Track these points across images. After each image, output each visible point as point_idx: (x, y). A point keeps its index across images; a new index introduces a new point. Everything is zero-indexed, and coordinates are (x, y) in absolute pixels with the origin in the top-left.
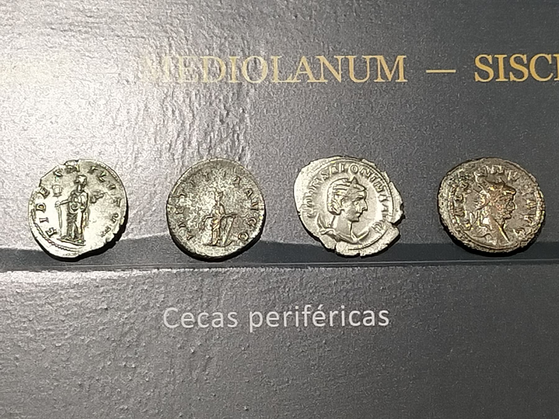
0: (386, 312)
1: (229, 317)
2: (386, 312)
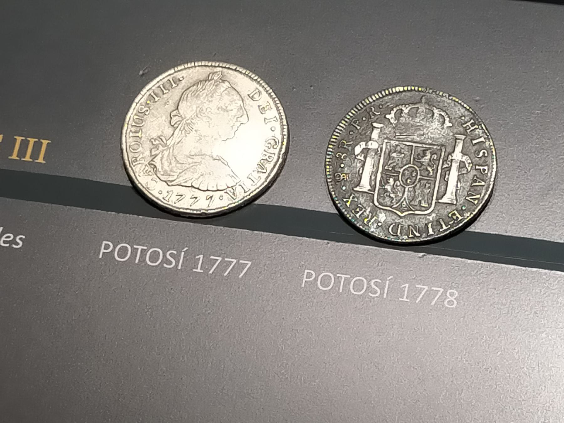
0: (24, 237)
2: (24, 237)
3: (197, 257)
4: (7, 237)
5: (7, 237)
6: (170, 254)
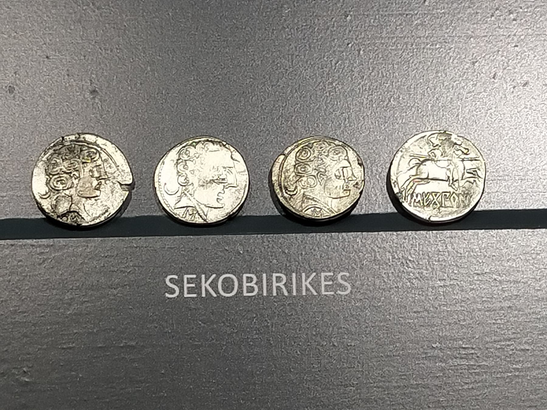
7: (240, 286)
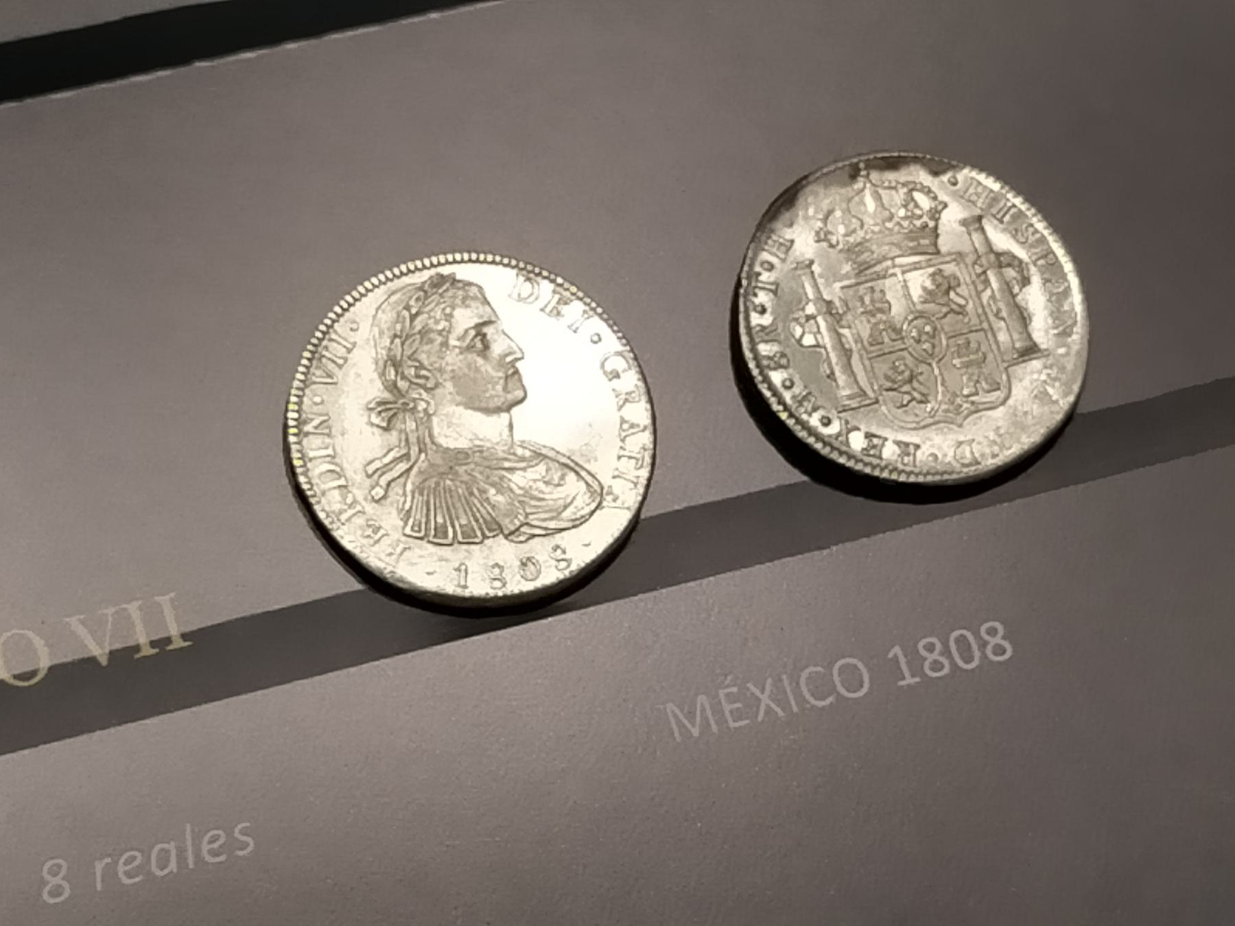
1: (237, 834)
3: (891, 655)
4: (210, 842)
5: (126, 863)
6: (246, 845)
7: (946, 652)
